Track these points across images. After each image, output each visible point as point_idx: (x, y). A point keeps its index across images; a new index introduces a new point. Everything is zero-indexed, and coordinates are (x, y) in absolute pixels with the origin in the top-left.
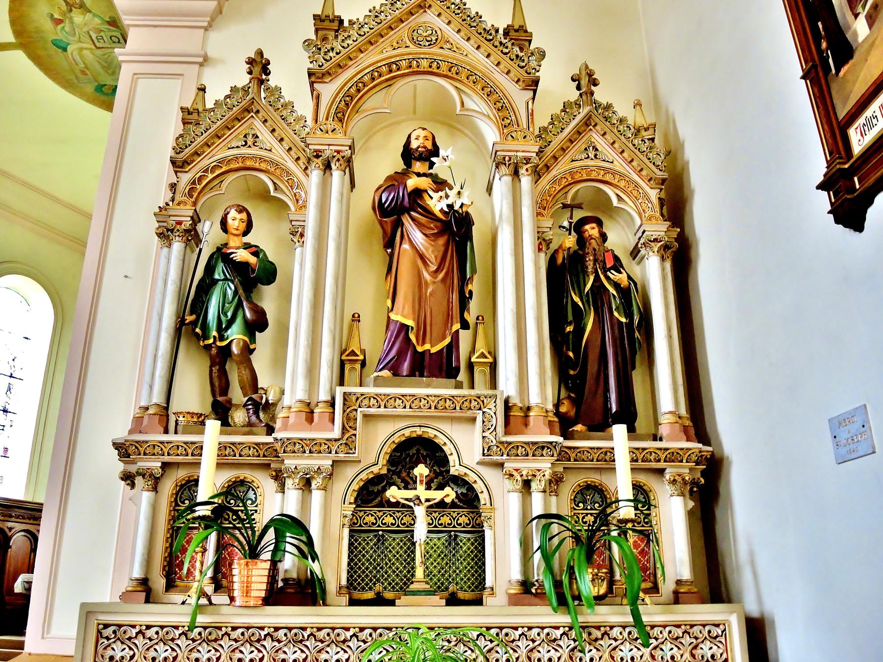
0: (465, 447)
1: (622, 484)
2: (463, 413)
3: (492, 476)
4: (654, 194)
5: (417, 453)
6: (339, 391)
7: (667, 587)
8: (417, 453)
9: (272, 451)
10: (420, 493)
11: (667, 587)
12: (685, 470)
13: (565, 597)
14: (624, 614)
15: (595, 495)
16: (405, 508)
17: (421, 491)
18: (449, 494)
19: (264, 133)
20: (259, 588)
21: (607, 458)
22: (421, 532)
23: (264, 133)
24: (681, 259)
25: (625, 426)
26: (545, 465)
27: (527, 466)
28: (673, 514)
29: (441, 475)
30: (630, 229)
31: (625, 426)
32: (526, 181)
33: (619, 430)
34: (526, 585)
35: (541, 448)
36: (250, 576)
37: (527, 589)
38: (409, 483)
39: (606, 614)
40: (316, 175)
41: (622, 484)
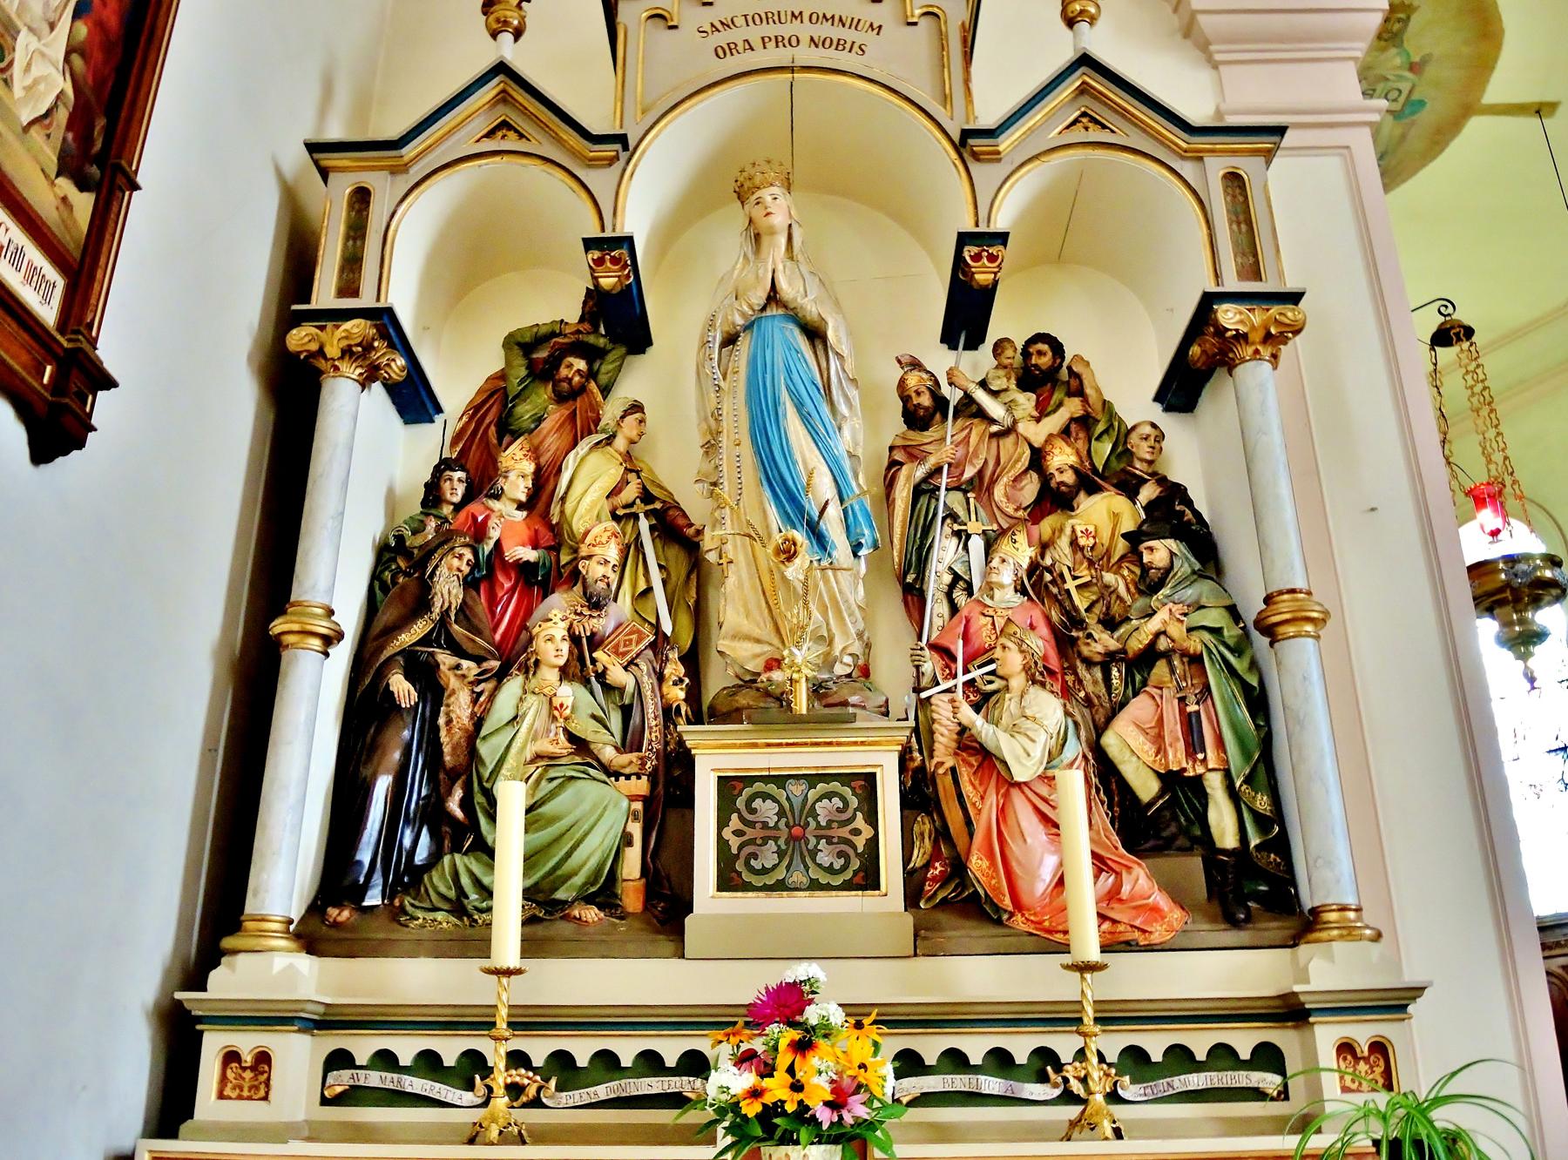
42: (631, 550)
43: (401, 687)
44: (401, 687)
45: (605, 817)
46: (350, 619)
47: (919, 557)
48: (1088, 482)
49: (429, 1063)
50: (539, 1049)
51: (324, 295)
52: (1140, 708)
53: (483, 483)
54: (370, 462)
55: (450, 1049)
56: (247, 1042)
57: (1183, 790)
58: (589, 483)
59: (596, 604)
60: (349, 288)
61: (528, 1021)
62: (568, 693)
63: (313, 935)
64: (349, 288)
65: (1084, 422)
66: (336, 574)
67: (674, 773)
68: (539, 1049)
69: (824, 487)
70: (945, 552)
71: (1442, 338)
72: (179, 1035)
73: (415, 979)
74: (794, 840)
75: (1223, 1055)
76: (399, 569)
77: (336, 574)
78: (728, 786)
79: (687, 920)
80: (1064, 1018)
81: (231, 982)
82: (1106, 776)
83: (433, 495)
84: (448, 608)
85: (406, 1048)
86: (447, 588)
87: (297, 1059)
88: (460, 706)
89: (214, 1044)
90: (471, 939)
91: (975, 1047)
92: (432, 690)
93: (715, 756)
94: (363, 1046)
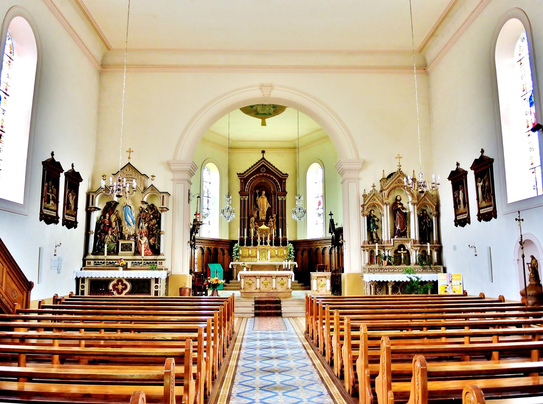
0: (408, 246)
1: (429, 250)
2: (408, 241)
3: (411, 250)
4: (434, 207)
5: (402, 246)
6: (392, 239)
7: (433, 263)
8: (402, 246)
9: (384, 247)
10: (402, 252)
11: (433, 263)
12: (437, 248)
13: (422, 265)
14: (394, 386)
15: (425, 252)
16: (400, 254)
17: (402, 251)
18: (406, 252)
19: (376, 199)
20: (386, 264)
21: (427, 247)
22: (402, 257)
23: (376, 199)
24: (438, 216)
25: (183, 372)
26: (419, 248)
27: (416, 248)
28: (435, 254)
29: (404, 250)
30: (430, 210)
31: (183, 372)
32: (416, 206)
33: (428, 244)
34: (416, 263)
35: (418, 246)
36: (385, 263)
37: (416, 264)
38: (401, 250)
39: (426, 266)
40: (385, 206)
41: (429, 250)
42: (116, 224)
43: (98, 236)
44: (98, 236)
45: (113, 245)
46: (94, 231)
47: (139, 225)
48: (153, 218)
49: (101, 262)
50: (108, 262)
51: (90, 205)
52: (153, 238)
53: (105, 217)
54: (96, 216)
55: (103, 262)
56: (160, 261)
57: (154, 245)
58: (113, 217)
59: (113, 229)
60: (92, 205)
61: (107, 260)
62: (111, 236)
63: (93, 254)
64: (92, 205)
65: (155, 212)
66: (93, 228)
67: (118, 243)
68: (108, 262)
69: (131, 221)
70: (141, 224)
71: (198, 197)
72: (84, 261)
73: (100, 257)
74: (126, 248)
75: (153, 263)
76: (98, 225)
77: (93, 228)
78: (122, 244)
79: (29, 280)
80: (141, 260)
81: (87, 257)
82: (149, 243)
83: (100, 218)
84: (102, 228)
85: (100, 261)
86: (102, 227)
87: (92, 262)
88: (103, 237)
89: (87, 261)
90: (104, 255)
91: (137, 262)
92: (101, 236)
93: (121, 242)
94: (97, 261)
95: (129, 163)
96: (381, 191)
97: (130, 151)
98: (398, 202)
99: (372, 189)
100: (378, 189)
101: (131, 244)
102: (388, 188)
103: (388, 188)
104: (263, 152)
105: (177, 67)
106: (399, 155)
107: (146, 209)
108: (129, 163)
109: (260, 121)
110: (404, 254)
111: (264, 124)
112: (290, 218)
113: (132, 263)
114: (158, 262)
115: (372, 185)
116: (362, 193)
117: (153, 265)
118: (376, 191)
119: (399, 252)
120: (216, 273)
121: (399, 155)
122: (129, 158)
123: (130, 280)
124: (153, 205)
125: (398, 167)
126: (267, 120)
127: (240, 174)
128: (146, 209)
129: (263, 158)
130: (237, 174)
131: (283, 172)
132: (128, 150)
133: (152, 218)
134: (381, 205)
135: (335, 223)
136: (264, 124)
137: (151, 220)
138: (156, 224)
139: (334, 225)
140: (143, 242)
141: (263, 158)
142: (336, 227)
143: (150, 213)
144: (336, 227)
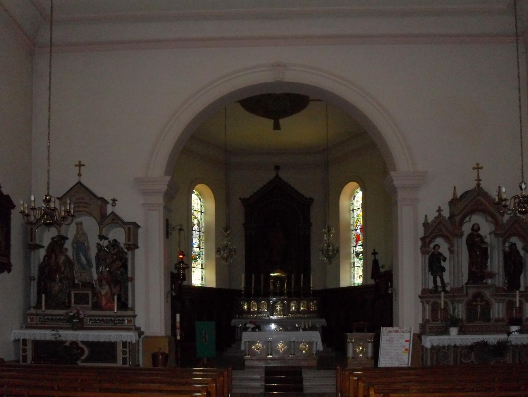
5: (478, 296)
8: (478, 296)
17: (479, 303)
18: (484, 303)
46: (36, 277)
76: (41, 268)
95: (79, 183)
96: (451, 218)
97: (80, 165)
98: (475, 233)
99: (436, 214)
100: (446, 213)
101: (88, 295)
102: (460, 212)
103: (460, 212)
104: (277, 168)
105: (159, 41)
106: (478, 164)
107: (106, 247)
108: (79, 183)
109: (271, 122)
110: (481, 306)
111: (277, 127)
112: (317, 259)
113: (91, 320)
114: (126, 319)
115: (437, 209)
116: (422, 220)
117: (116, 324)
118: (444, 217)
119: (474, 303)
120: (206, 331)
121: (478, 164)
122: (79, 175)
123: (88, 344)
124: (115, 241)
125: (476, 182)
126: (282, 121)
127: (245, 199)
128: (106, 247)
129: (277, 177)
130: (240, 199)
131: (306, 196)
132: (77, 163)
133: (117, 264)
134: (451, 238)
135: (380, 265)
136: (277, 127)
137: (113, 262)
138: (121, 267)
139: (379, 268)
140: (103, 292)
141: (277, 177)
142: (382, 270)
143: (113, 252)
144: (382, 270)
